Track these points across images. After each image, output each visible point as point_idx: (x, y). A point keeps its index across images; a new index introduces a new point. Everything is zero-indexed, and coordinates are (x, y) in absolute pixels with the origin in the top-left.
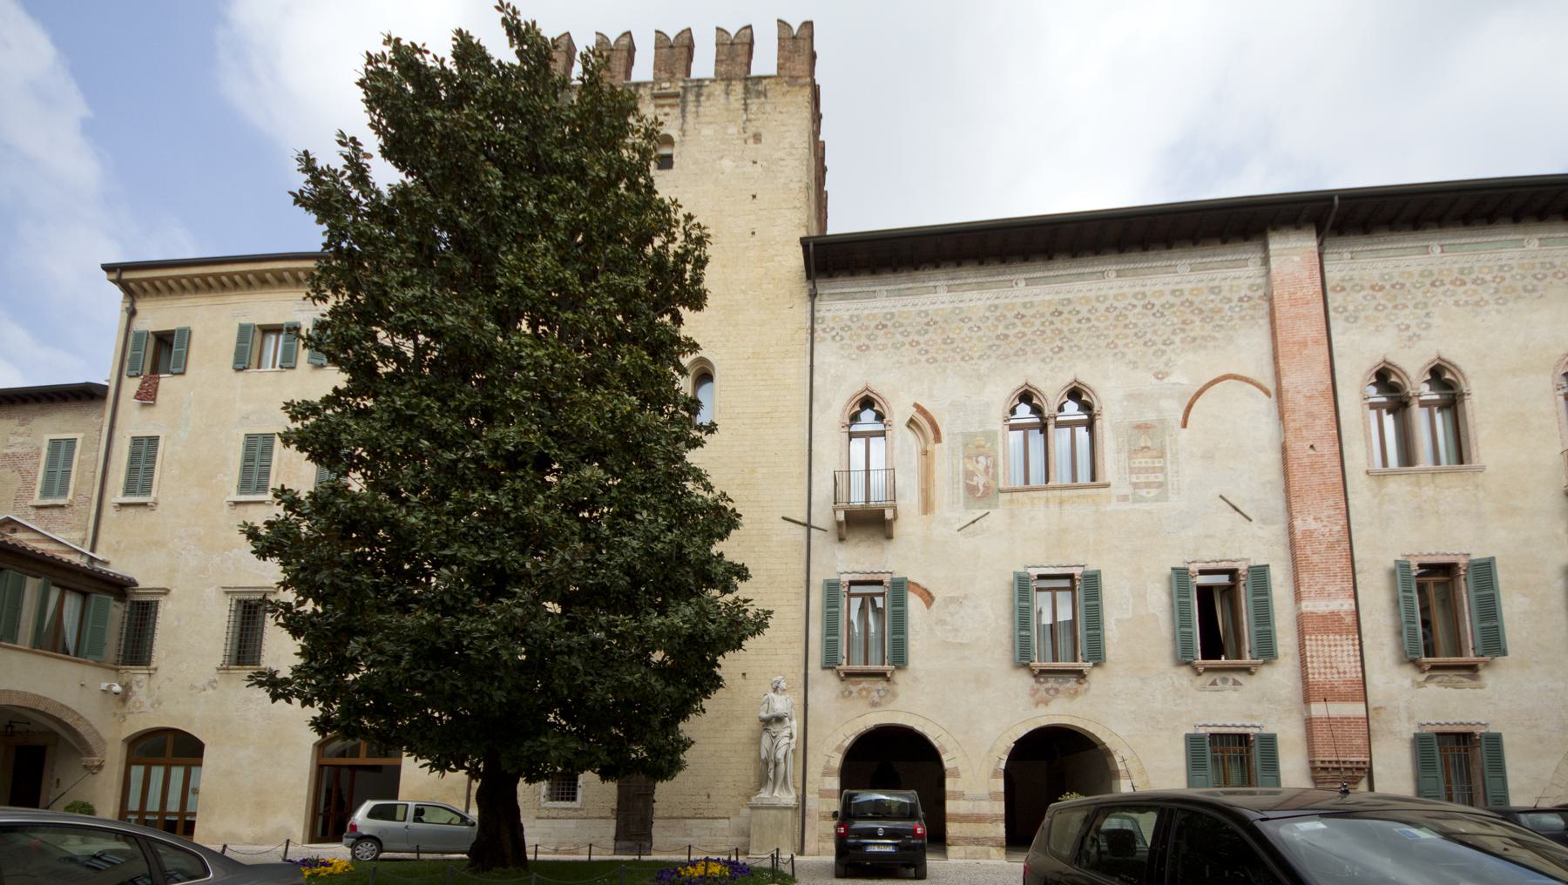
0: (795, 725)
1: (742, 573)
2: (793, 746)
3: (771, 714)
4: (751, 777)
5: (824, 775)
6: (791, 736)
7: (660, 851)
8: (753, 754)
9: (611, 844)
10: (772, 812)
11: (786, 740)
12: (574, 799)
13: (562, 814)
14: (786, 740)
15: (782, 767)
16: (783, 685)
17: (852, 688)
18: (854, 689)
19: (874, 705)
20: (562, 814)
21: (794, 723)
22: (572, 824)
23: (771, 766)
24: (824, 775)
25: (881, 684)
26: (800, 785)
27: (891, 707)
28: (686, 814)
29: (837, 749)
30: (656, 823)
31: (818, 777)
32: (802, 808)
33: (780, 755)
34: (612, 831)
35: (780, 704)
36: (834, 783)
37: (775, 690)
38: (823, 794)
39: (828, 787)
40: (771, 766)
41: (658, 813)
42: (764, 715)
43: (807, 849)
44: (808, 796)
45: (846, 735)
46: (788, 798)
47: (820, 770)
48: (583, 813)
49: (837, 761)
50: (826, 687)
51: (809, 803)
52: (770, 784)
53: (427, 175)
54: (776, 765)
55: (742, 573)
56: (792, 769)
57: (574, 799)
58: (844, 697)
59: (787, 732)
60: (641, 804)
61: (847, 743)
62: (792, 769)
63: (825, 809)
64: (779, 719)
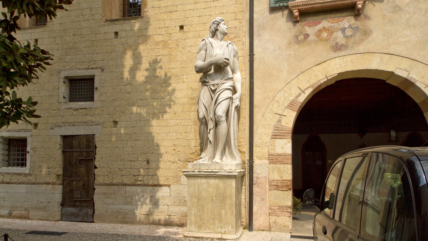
0: (239, 78)
1: (2, 154)
2: (237, 102)
3: (208, 61)
4: (194, 142)
5: (275, 136)
6: (234, 90)
7: (103, 220)
8: (193, 115)
9: (57, 209)
10: (212, 181)
11: (228, 94)
12: (23, 165)
13: (15, 179)
14: (228, 94)
15: (223, 126)
16: (223, 27)
17: (309, 30)
18: (311, 31)
19: (337, 48)
20: (15, 179)
21: (238, 76)
22: (22, 188)
23: (211, 125)
24: (275, 136)
25: (347, 21)
26: (246, 149)
27: (362, 48)
28: (126, 181)
29: (290, 106)
30: (98, 190)
31: (267, 139)
32: (247, 177)
33: (221, 111)
34: (58, 197)
35: (220, 50)
36: (285, 146)
37: (214, 34)
38: (274, 159)
39: (279, 151)
40: (211, 125)
41: (99, 179)
42: (200, 63)
43: (256, 223)
44: (256, 162)
45: (300, 87)
46: (232, 164)
47: (270, 131)
48: (32, 179)
49: (289, 120)
50: (275, 33)
51: (256, 170)
52: (210, 148)
53: (319, 163)
54: (217, 124)
55: (2, 154)
56: (238, 131)
57: (23, 165)
58: (298, 42)
59: (228, 84)
60: (83, 170)
61: (302, 98)
62: (238, 131)
63: (276, 176)
64: (220, 68)
